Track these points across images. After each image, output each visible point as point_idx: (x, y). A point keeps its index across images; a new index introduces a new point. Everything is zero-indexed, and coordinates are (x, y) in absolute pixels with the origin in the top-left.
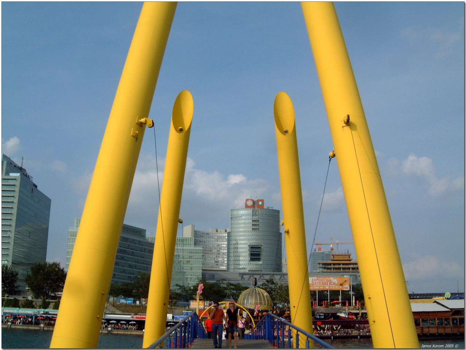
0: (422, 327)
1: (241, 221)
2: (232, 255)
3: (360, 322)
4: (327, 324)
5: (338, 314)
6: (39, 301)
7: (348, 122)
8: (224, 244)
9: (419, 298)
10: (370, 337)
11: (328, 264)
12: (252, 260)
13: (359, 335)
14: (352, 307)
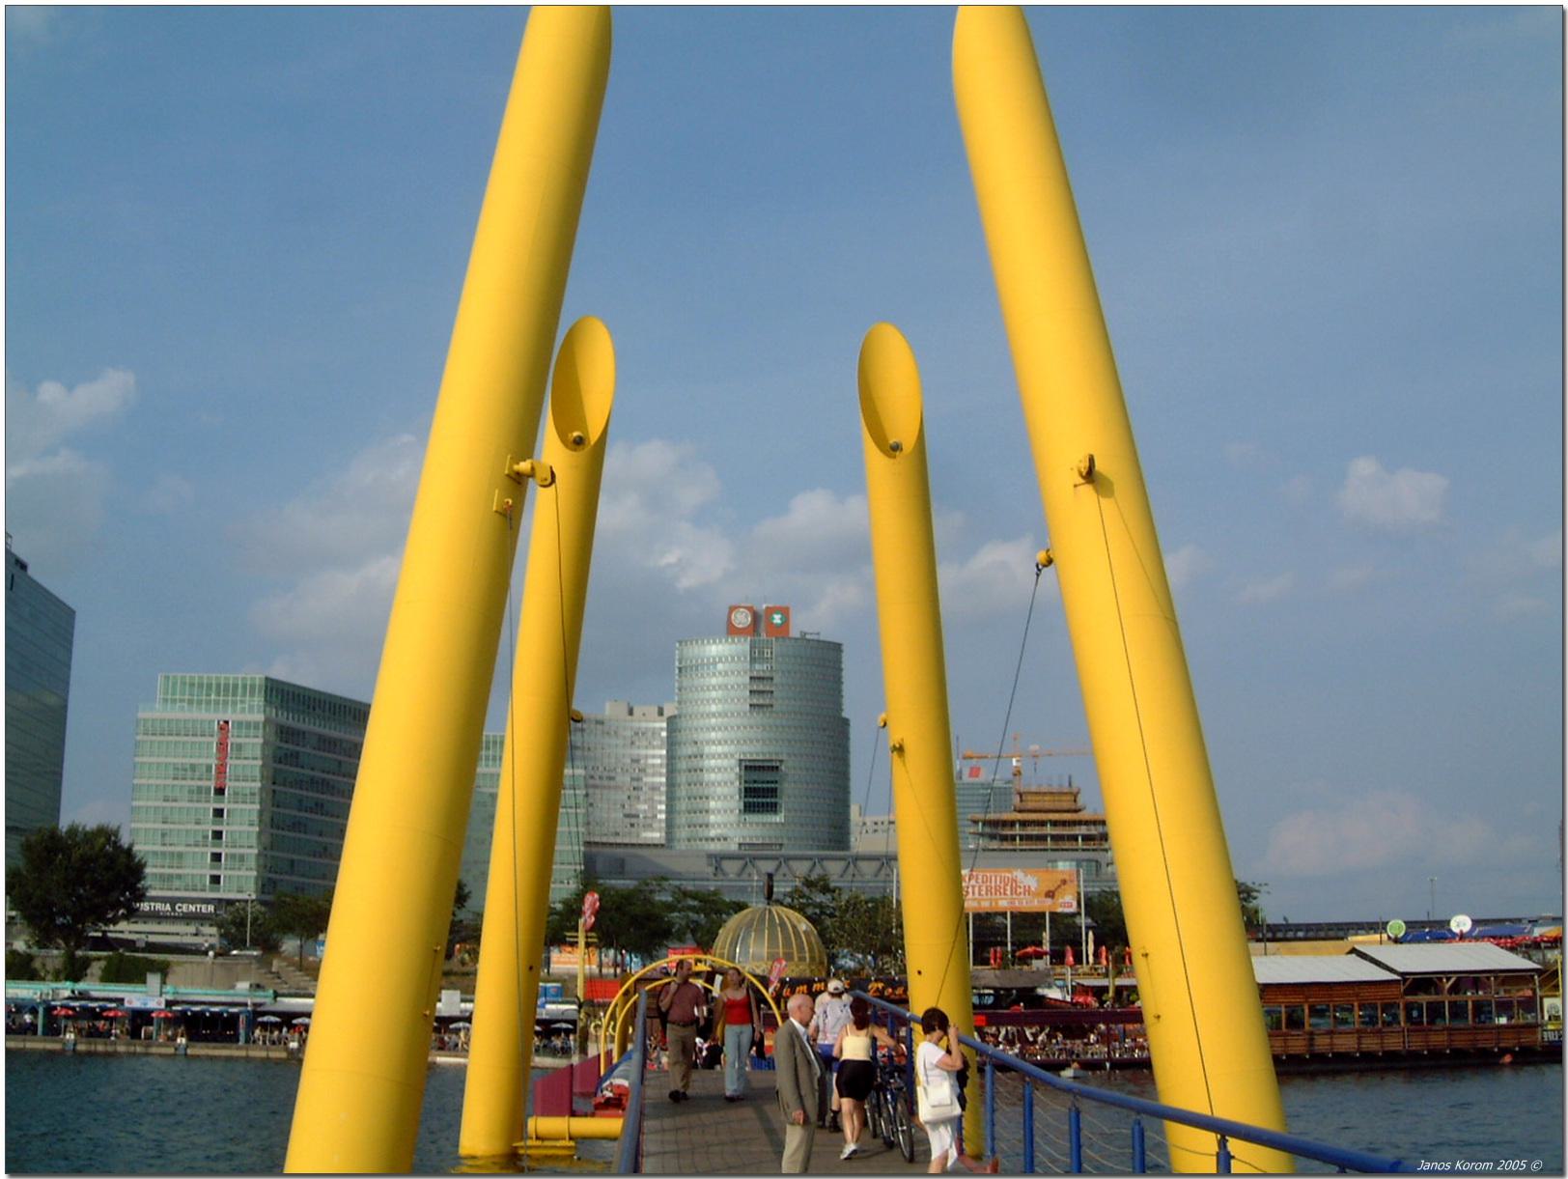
0: (1312, 1033)
1: (714, 681)
2: (682, 792)
3: (1110, 1018)
4: (1003, 1024)
5: (1040, 991)
6: (55, 956)
7: (1090, 475)
8: (657, 756)
9: (1306, 939)
10: (1146, 1064)
11: (1005, 824)
12: (749, 808)
13: (1109, 1059)
14: (1085, 968)
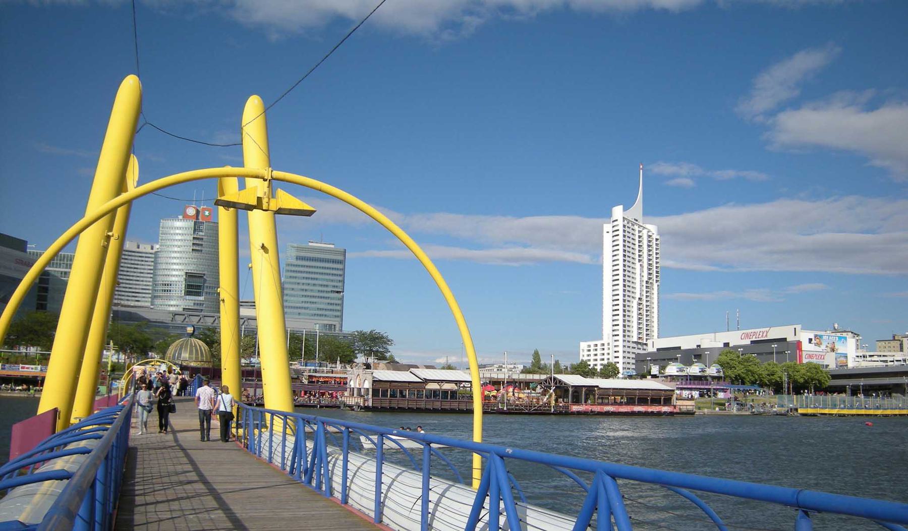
12: (188, 293)
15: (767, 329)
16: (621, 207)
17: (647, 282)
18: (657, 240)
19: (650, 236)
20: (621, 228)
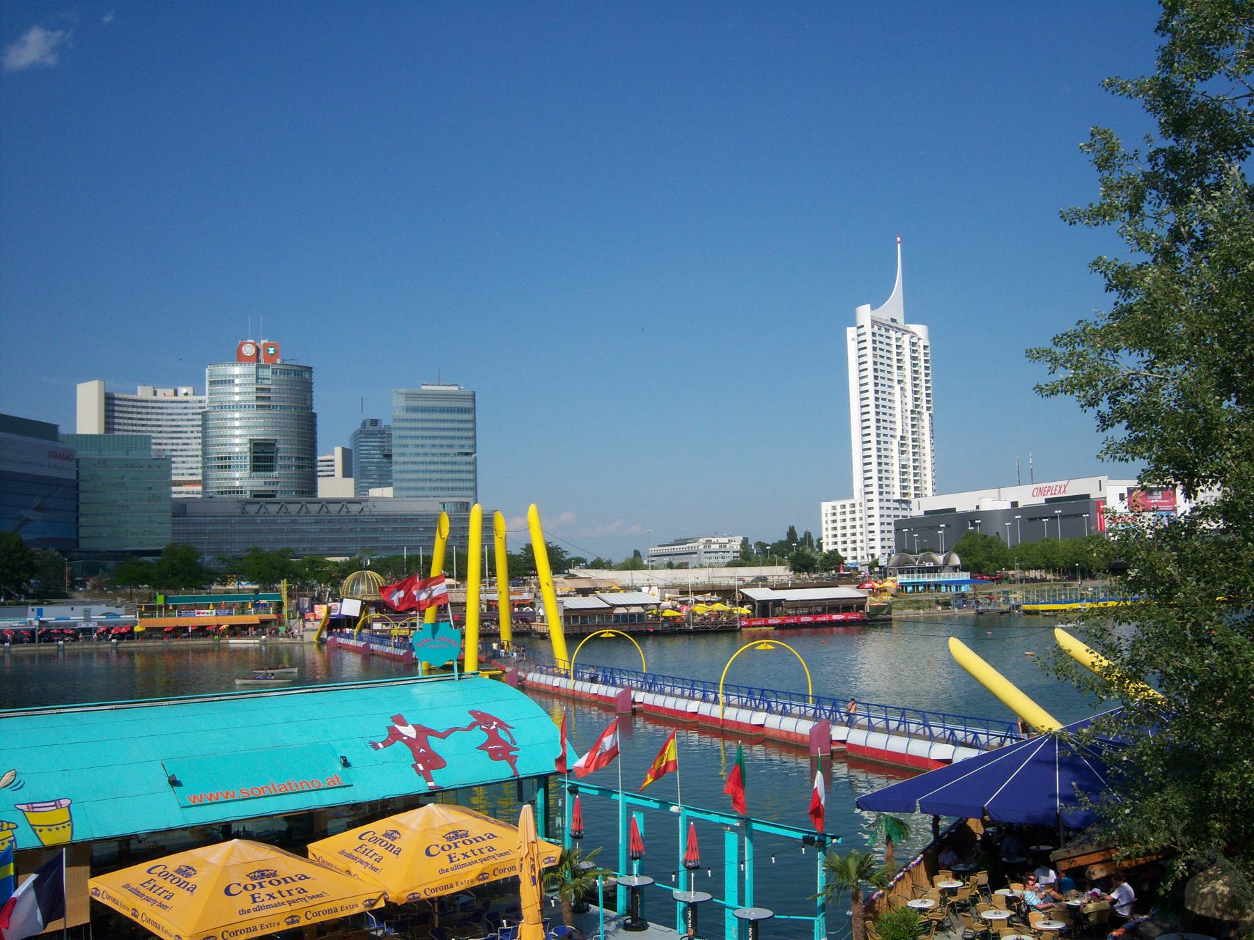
12: (255, 468)
15: (1065, 482)
16: (868, 306)
17: (912, 412)
18: (925, 347)
19: (914, 344)
20: (869, 337)
